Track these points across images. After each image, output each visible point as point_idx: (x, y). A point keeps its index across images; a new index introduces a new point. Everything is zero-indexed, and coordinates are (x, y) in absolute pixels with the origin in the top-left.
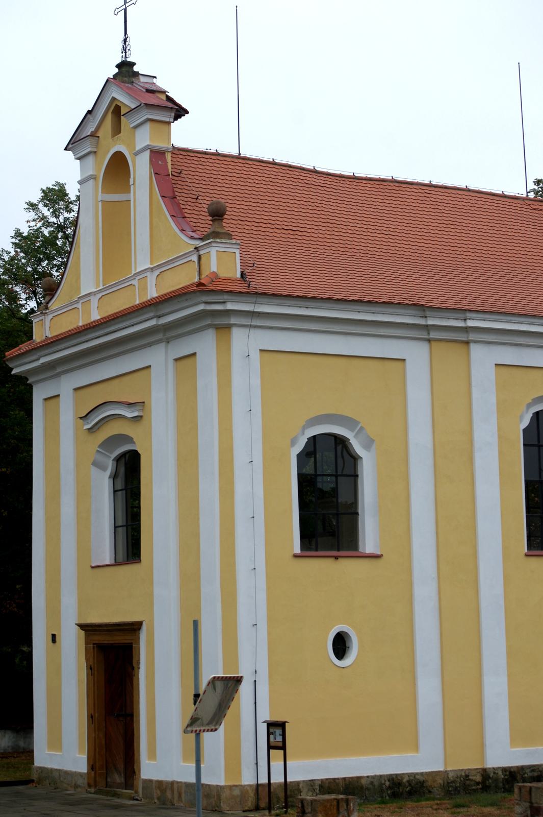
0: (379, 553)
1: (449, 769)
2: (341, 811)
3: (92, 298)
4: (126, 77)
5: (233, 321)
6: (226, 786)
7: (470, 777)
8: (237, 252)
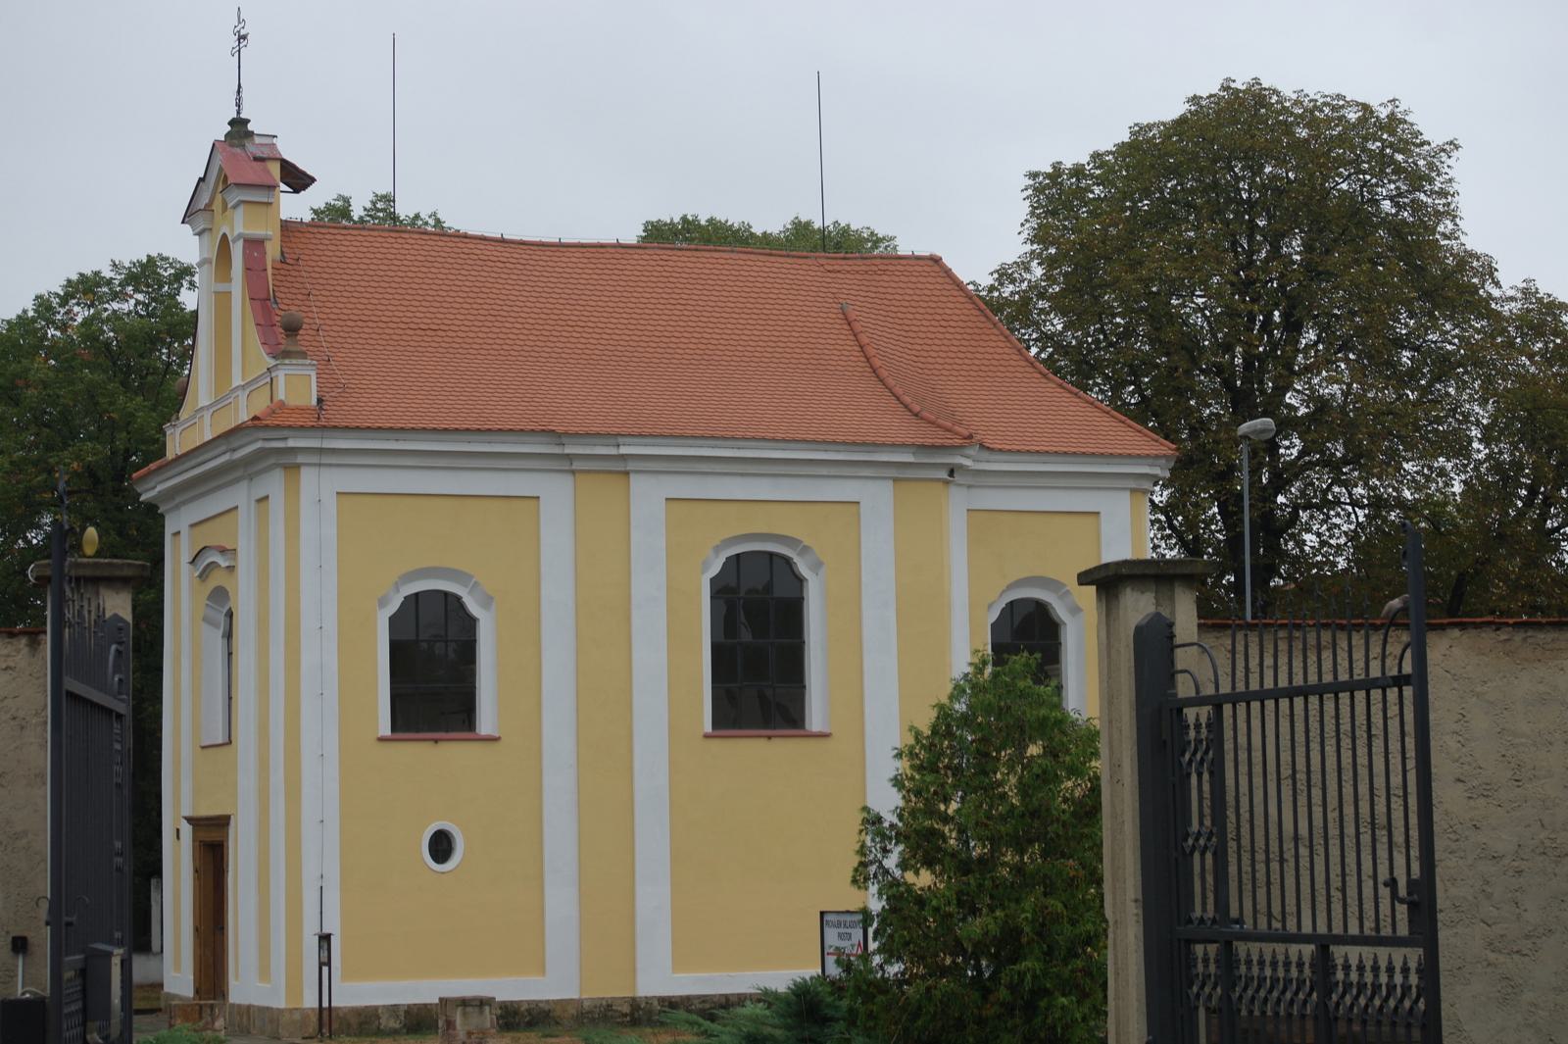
0: (497, 735)
1: (584, 997)
2: (204, 1015)
3: (205, 413)
4: (235, 139)
5: (300, 459)
6: (286, 1009)
7: (614, 1008)
8: (313, 375)
